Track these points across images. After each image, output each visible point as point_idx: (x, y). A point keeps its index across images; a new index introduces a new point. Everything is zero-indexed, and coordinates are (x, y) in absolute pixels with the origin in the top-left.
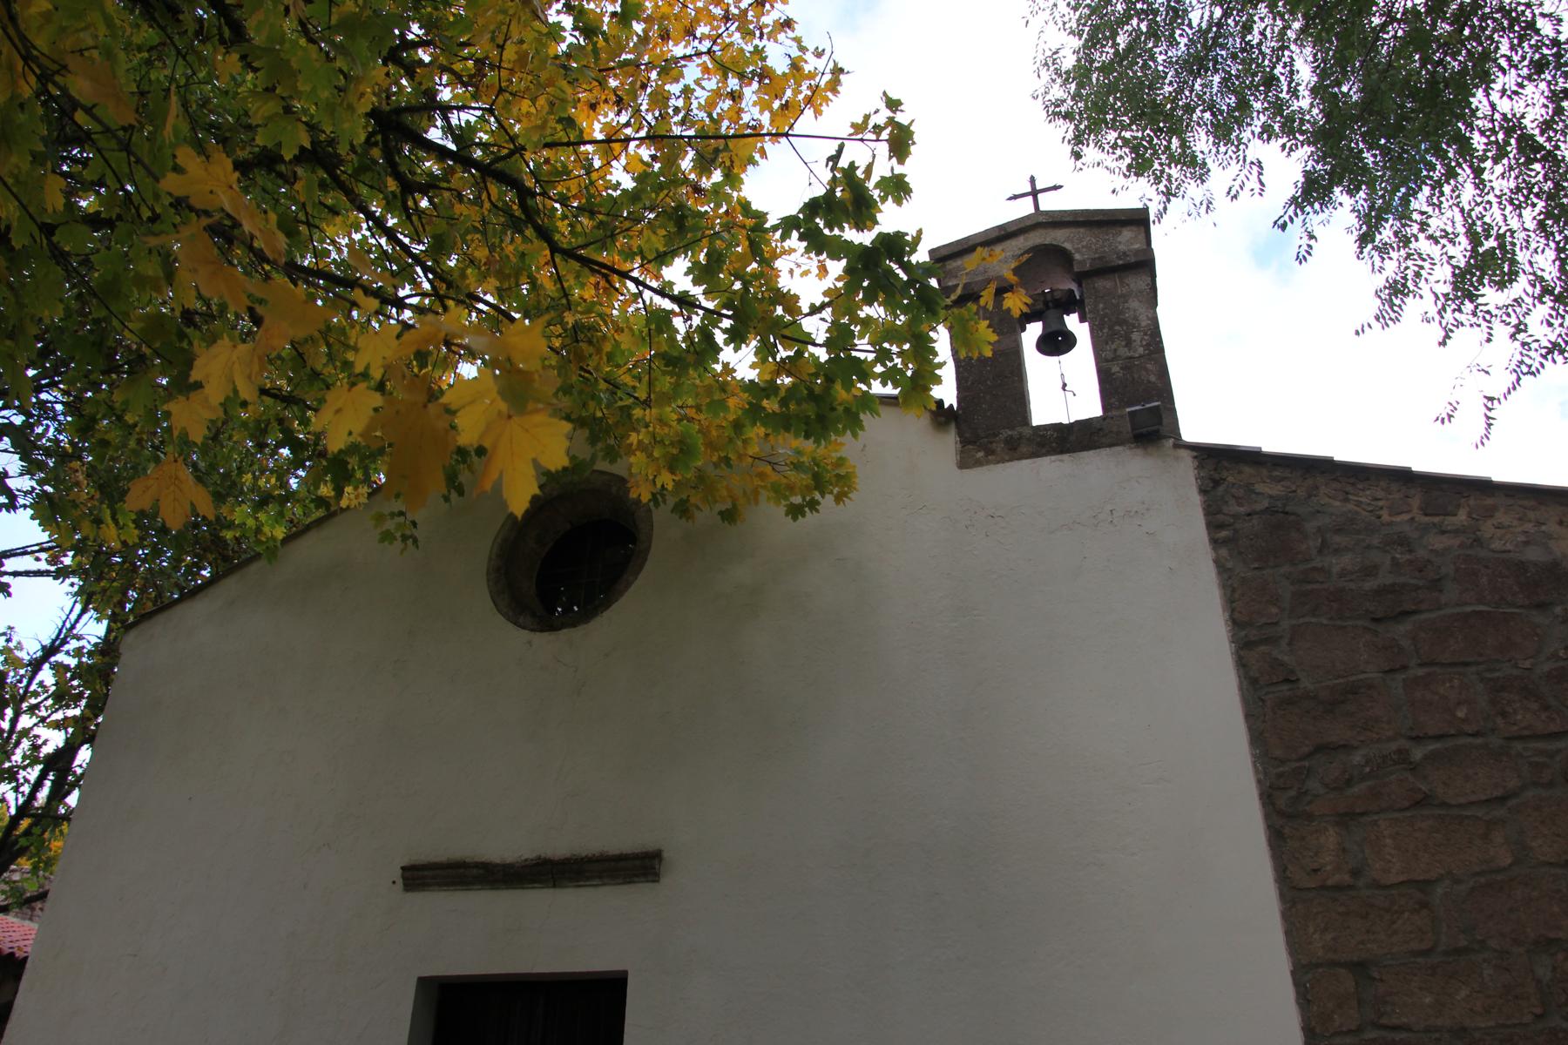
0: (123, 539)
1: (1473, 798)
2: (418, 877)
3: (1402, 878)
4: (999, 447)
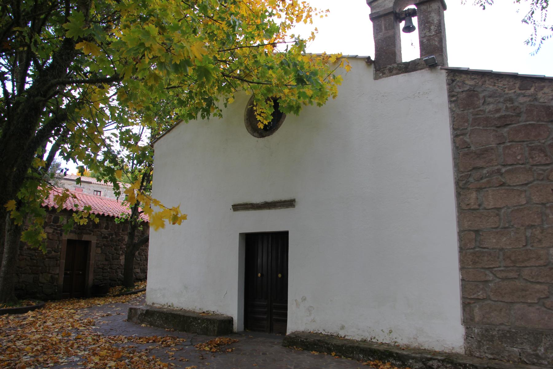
1: (518, 184)
2: (236, 207)
3: (493, 207)
4: (387, 71)
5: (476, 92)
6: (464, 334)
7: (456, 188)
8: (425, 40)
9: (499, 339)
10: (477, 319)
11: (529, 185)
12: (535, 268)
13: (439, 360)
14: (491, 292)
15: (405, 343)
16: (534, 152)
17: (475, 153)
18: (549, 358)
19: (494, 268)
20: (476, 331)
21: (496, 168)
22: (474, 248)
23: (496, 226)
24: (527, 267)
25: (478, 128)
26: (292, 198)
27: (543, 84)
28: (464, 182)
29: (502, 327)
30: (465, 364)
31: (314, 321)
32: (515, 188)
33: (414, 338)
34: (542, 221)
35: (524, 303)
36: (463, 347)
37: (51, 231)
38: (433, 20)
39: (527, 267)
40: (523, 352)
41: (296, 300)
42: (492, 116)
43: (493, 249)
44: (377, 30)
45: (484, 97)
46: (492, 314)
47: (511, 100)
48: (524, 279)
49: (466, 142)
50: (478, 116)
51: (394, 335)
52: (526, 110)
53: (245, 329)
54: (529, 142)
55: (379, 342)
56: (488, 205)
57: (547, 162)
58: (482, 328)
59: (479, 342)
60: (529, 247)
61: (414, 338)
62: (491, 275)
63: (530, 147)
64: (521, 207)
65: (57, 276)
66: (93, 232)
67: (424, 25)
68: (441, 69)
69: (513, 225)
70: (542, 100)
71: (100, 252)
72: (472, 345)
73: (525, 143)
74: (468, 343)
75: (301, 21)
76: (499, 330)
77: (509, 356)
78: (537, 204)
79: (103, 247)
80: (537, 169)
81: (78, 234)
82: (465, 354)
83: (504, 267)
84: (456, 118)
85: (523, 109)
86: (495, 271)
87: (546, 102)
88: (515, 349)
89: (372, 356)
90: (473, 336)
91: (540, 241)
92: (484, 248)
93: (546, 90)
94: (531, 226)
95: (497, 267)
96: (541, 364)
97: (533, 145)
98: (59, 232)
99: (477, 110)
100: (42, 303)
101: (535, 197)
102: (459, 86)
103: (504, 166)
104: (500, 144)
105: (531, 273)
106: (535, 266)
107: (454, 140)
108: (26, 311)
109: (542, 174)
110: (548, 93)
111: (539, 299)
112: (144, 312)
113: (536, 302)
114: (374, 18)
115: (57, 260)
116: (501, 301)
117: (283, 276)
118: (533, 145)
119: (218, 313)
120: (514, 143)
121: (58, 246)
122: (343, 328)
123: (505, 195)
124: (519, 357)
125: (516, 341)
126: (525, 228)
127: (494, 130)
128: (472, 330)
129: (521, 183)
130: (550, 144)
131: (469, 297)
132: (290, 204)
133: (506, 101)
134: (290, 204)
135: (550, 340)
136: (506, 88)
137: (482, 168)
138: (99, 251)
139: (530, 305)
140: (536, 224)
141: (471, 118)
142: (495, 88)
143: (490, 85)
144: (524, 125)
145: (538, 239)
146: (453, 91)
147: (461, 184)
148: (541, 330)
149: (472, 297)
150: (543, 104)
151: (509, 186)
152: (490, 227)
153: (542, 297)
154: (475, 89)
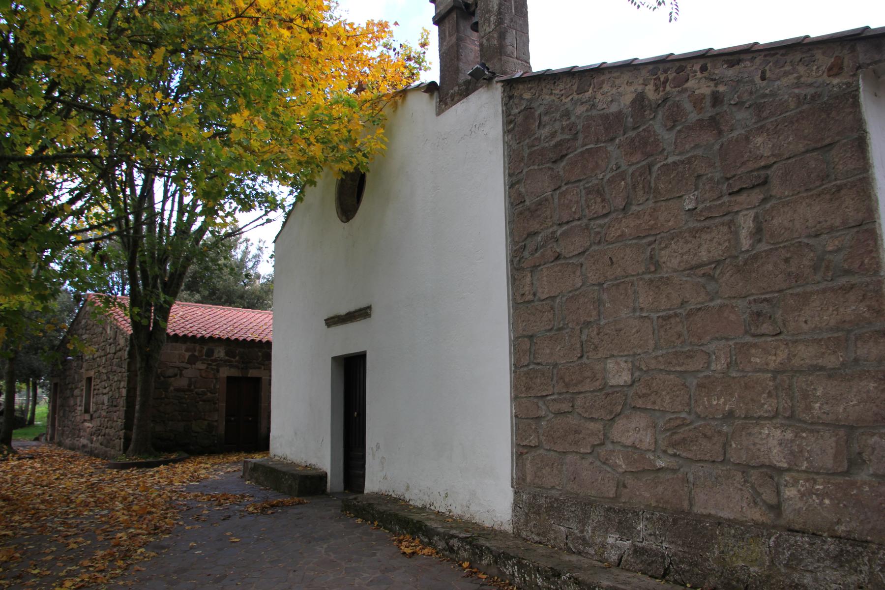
0: (52, 61)
1: (574, 253)
2: (333, 321)
3: (547, 296)
4: (449, 100)
5: (533, 110)
10: (528, 480)
12: (589, 394)
17: (529, 209)
19: (547, 396)
21: (551, 230)
23: (550, 327)
28: (518, 258)
29: (554, 492)
31: (385, 478)
34: (599, 314)
37: (203, 367)
38: (493, 7)
39: (582, 392)
42: (547, 145)
45: (540, 115)
46: (544, 471)
47: (567, 114)
49: (520, 194)
51: (450, 501)
53: (345, 489)
54: (585, 181)
57: (605, 212)
58: (529, 493)
59: (527, 514)
60: (585, 360)
62: (544, 407)
63: (588, 188)
64: (577, 293)
65: (215, 424)
66: (263, 365)
68: (497, 82)
72: (519, 519)
73: (582, 183)
74: (516, 516)
76: (546, 498)
77: (555, 538)
81: (242, 369)
88: (562, 528)
89: (406, 529)
91: (596, 348)
92: (538, 364)
93: (606, 88)
94: (588, 324)
98: (215, 367)
100: (186, 455)
101: (591, 273)
103: (560, 225)
108: (158, 464)
109: (599, 233)
110: (607, 92)
115: (215, 404)
117: (359, 415)
119: (317, 467)
120: (570, 186)
121: (215, 387)
129: (577, 253)
132: (363, 313)
134: (363, 313)
136: (562, 95)
137: (536, 233)
139: (584, 456)
140: (592, 320)
141: (526, 152)
142: (552, 97)
149: (524, 444)
150: (601, 112)
151: (565, 258)
152: (543, 329)
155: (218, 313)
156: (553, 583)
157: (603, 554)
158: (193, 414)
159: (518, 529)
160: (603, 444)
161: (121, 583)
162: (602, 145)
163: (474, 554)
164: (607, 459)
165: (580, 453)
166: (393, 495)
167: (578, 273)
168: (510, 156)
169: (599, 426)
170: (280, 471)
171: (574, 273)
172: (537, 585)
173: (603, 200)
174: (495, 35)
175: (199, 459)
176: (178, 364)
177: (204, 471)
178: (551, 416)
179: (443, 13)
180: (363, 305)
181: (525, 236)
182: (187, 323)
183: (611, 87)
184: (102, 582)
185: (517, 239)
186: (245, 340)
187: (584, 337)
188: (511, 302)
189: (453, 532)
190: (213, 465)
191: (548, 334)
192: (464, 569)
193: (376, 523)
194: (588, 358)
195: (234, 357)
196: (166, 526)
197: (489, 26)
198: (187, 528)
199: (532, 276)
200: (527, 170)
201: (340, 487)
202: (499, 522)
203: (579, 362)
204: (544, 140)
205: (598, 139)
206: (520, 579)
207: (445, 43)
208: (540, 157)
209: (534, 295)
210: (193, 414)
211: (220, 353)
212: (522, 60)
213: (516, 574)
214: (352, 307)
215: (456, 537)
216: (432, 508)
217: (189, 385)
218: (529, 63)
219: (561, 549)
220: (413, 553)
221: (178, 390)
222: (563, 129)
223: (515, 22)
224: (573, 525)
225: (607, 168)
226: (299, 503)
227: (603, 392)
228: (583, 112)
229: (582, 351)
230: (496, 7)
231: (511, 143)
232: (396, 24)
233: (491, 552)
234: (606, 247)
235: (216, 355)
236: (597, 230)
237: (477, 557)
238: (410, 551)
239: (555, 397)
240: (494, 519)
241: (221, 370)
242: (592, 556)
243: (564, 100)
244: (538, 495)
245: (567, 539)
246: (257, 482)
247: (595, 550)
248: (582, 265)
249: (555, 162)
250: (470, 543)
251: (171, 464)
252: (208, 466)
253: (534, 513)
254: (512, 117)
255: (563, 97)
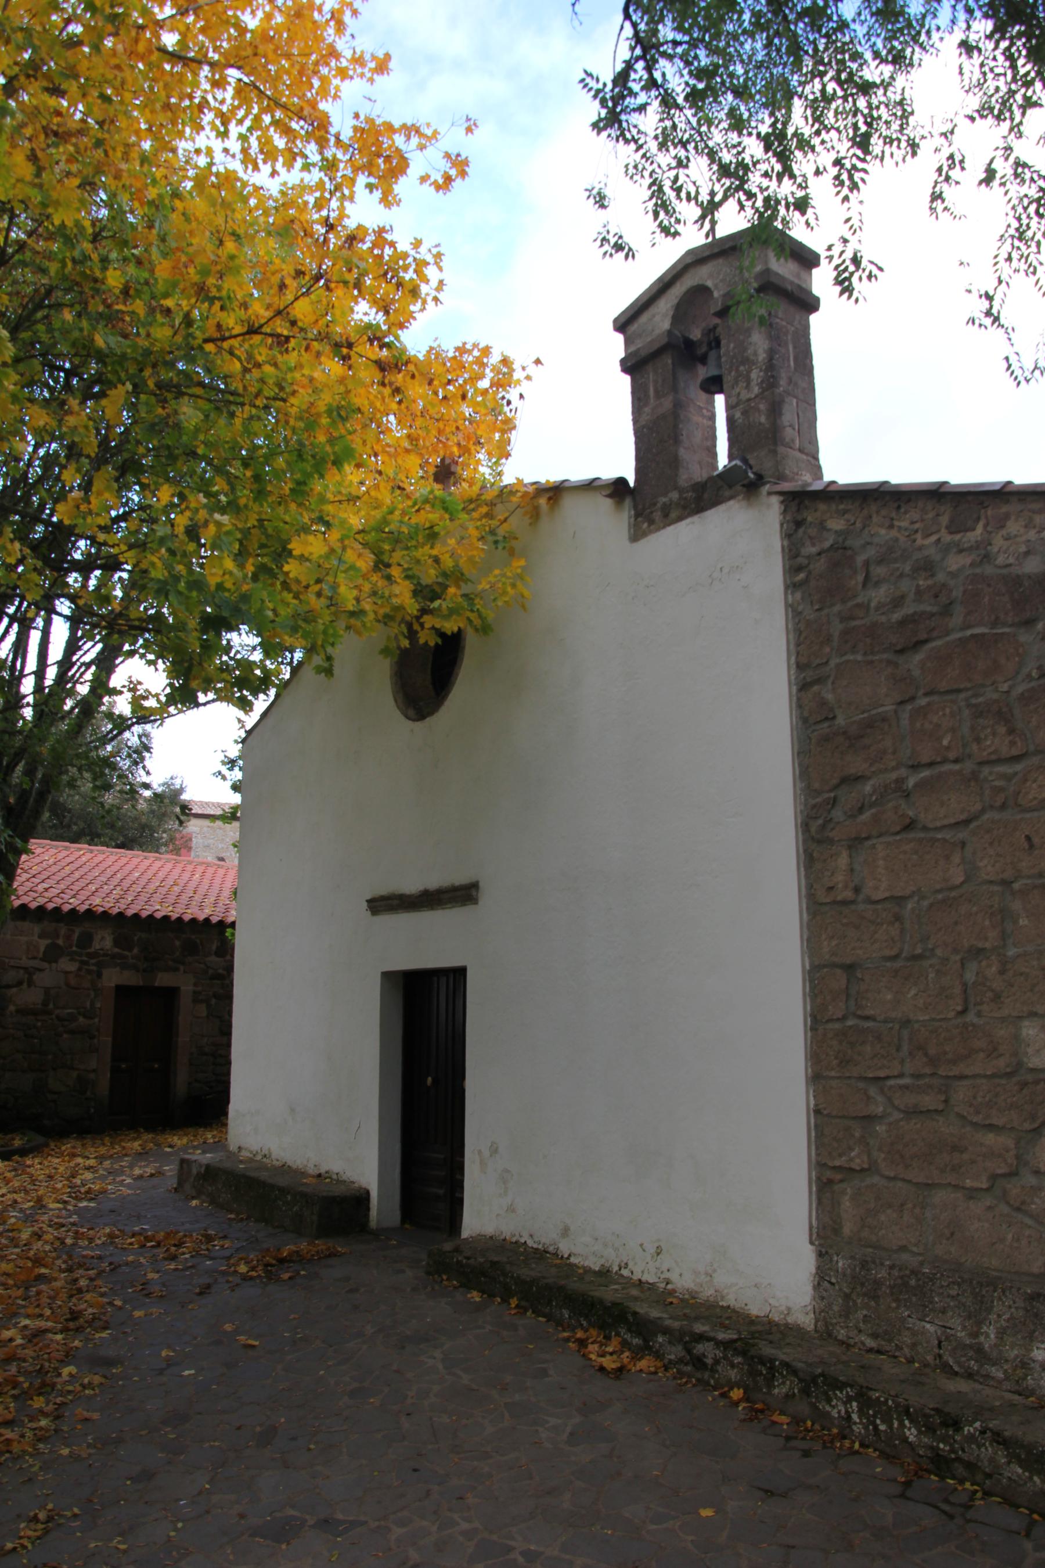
1: (946, 822)
3: (887, 894)
4: (657, 515)
5: (849, 552)
6: (814, 1271)
7: (804, 841)
8: (738, 415)
9: (892, 1294)
10: (847, 1229)
11: (973, 825)
12: (984, 1081)
13: (718, 1343)
14: (880, 1150)
15: (686, 1285)
16: (981, 721)
17: (845, 733)
18: (1007, 1361)
19: (888, 1078)
20: (840, 1264)
21: (894, 776)
22: (844, 1018)
23: (893, 953)
24: (966, 1077)
25: (851, 657)
26: (474, 880)
27: (1004, 509)
28: (820, 821)
29: (905, 1256)
30: (772, 1361)
31: (511, 1209)
32: (939, 836)
33: (707, 1274)
34: (1004, 936)
35: (956, 1186)
36: (810, 1308)
37: (73, 967)
38: (755, 354)
39: (966, 1077)
40: (947, 1338)
41: (480, 1152)
42: (883, 619)
43: (885, 1021)
44: (639, 399)
45: (867, 564)
46: (883, 1218)
47: (927, 567)
48: (960, 1116)
49: (823, 703)
50: (854, 623)
52: (965, 592)
53: (403, 1220)
54: (970, 693)
55: (635, 1277)
56: (877, 888)
57: (1015, 752)
58: (852, 1258)
59: (847, 1297)
60: (971, 1017)
61: (707, 1274)
62: (880, 1099)
63: (975, 705)
64: (953, 894)
65: (92, 1076)
67: (737, 370)
68: (770, 494)
69: (933, 950)
70: (1001, 560)
71: (205, 1014)
72: (830, 1305)
73: (962, 696)
74: (823, 1298)
75: (811, 305)
76: (892, 1267)
77: (914, 1345)
78: (991, 882)
79: (213, 1001)
80: (990, 773)
82: (816, 1331)
83: (912, 1076)
84: (804, 635)
85: (957, 593)
86: (891, 1087)
87: (1010, 565)
88: (928, 1326)
89: (586, 1317)
90: (833, 1280)
91: (997, 997)
92: (867, 1018)
93: (1013, 527)
94: (978, 953)
95: (895, 1077)
96: (987, 1376)
97: (981, 700)
98: (94, 968)
99: (850, 604)
100: (41, 1139)
101: (985, 862)
102: (810, 538)
103: (915, 767)
104: (902, 703)
105: (975, 1098)
106: (985, 1076)
107: (799, 699)
109: (1001, 789)
110: (1016, 536)
111: (994, 1177)
112: (203, 1170)
113: (984, 1186)
114: (631, 366)
116: (903, 1180)
118: (981, 700)
119: (344, 1178)
120: (935, 698)
122: (566, 1232)
123: (915, 857)
124: (936, 1350)
125: (931, 1302)
126: (962, 960)
127: (889, 662)
128: (831, 1261)
129: (952, 821)
130: (1022, 694)
131: (830, 1164)
133: (916, 569)
135: (1010, 1307)
136: (916, 531)
137: (859, 779)
138: (202, 1010)
139: (972, 1194)
140: (987, 945)
141: (837, 628)
142: (894, 533)
143: (881, 526)
144: (960, 639)
145: (993, 991)
146: (797, 556)
147: (814, 827)
148: (995, 1274)
149: (837, 1163)
150: (1005, 571)
151: (925, 828)
153: (999, 1171)
154: (848, 543)
155: (84, 859)
156: (944, 1439)
157: (1025, 1378)
158: (50, 1057)
159: (826, 1325)
160: (1013, 1174)
161: (65, 1451)
162: (1007, 630)
163: (753, 1373)
164: (1023, 1203)
165: (963, 1188)
166: (530, 1243)
167: (956, 859)
168: (799, 632)
169: (1006, 1141)
170: (273, 1187)
171: (947, 858)
172: (905, 1440)
173: (1011, 731)
174: (762, 407)
175: (67, 1147)
176: (25, 962)
177: (88, 1175)
178: (897, 1115)
179: (643, 353)
180: (459, 878)
181: (835, 782)
182: (36, 881)
183: (1026, 526)
184: (24, 1451)
185: (816, 785)
186: (151, 917)
187: (970, 976)
188: (804, 901)
189: (700, 1328)
190: (101, 1159)
191: (888, 964)
192: (736, 1404)
193: (514, 1302)
194: (979, 1014)
195: (130, 950)
196: (90, 1310)
197: (748, 387)
198: (138, 1314)
199: (850, 856)
200: (838, 661)
201: (394, 1217)
202: (783, 1308)
203: (959, 1020)
204: (877, 609)
205: (997, 618)
206: (866, 1428)
207: (647, 410)
208: (868, 640)
209: (857, 890)
210: (50, 1057)
211: (104, 941)
212: (807, 454)
213: (855, 1417)
214: (434, 881)
215: (709, 1339)
216: (625, 1272)
217: (45, 1003)
218: (817, 459)
219: (926, 1365)
220: (621, 1369)
221: (21, 1012)
222: (919, 592)
223: (796, 384)
224: (955, 1322)
225: (1018, 673)
226: (332, 1255)
227: (1015, 1079)
228: (964, 566)
229: (966, 1001)
230: (762, 356)
231: (800, 608)
232: (538, 362)
233: (795, 1372)
234: (1019, 817)
235: (96, 945)
236: (997, 783)
237: (760, 1379)
238: (614, 1366)
239: (906, 1081)
240: (771, 1301)
241: (106, 973)
242: (1000, 1382)
243: (919, 541)
244: (874, 1262)
245: (940, 1346)
246: (213, 1201)
247: (1005, 1372)
248: (963, 844)
249: (901, 652)
250: (744, 1353)
251: (16, 1157)
252: (92, 1162)
253: (865, 1295)
254: (800, 560)
255: (919, 536)
